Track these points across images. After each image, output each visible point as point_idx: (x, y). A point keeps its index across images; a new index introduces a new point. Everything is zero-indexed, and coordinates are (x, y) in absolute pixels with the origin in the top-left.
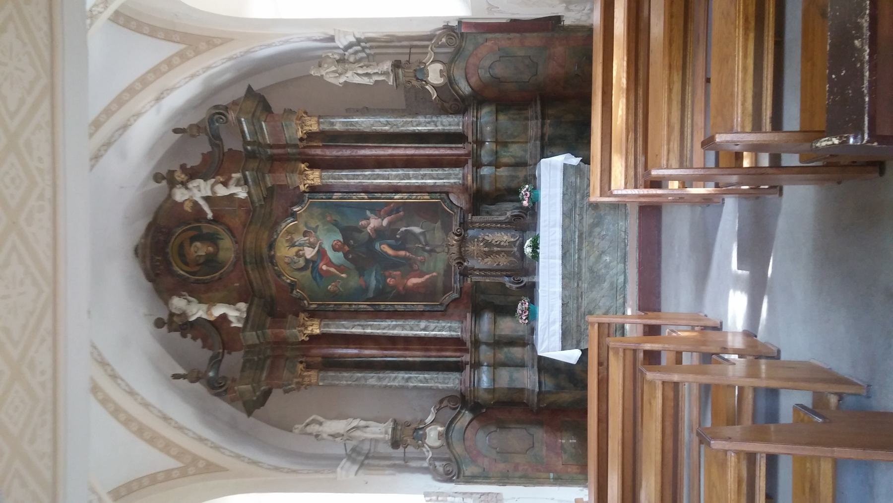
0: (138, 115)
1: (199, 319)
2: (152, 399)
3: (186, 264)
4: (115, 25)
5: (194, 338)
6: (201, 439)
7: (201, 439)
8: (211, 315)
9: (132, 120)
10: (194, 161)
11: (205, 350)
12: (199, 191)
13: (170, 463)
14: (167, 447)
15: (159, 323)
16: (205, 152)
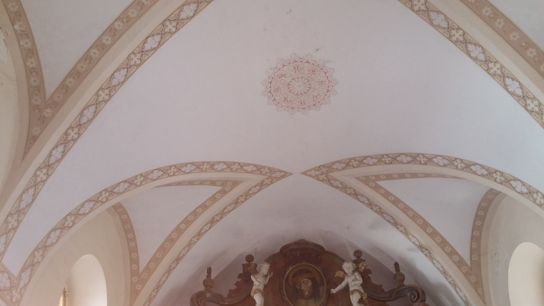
0: (406, 233)
1: (252, 283)
2: (195, 249)
3: (294, 276)
4: (476, 207)
5: (237, 284)
6: (158, 287)
7: (158, 287)
8: (255, 293)
9: (402, 229)
10: (375, 279)
11: (228, 292)
12: (353, 282)
13: (144, 259)
14: (156, 260)
15: (250, 258)
16: (383, 287)
